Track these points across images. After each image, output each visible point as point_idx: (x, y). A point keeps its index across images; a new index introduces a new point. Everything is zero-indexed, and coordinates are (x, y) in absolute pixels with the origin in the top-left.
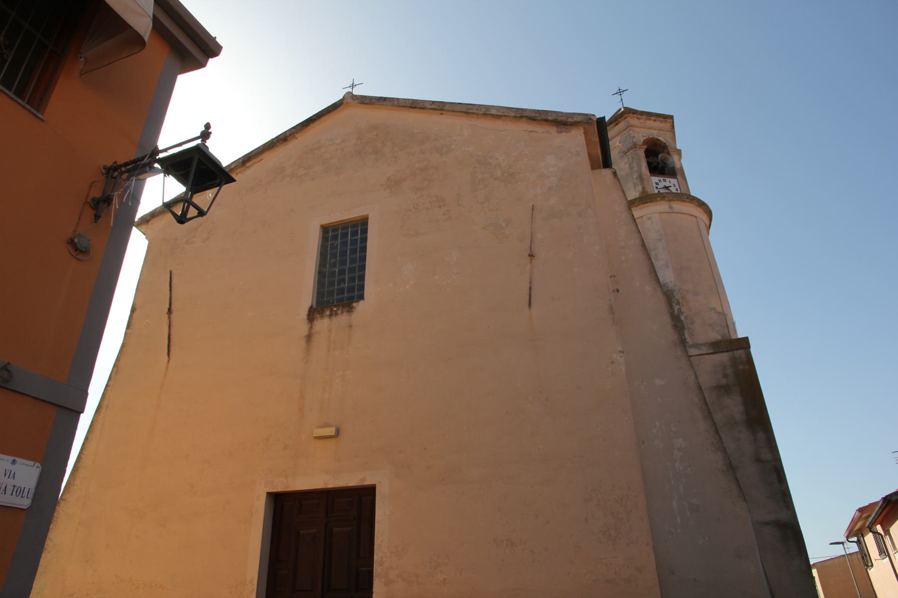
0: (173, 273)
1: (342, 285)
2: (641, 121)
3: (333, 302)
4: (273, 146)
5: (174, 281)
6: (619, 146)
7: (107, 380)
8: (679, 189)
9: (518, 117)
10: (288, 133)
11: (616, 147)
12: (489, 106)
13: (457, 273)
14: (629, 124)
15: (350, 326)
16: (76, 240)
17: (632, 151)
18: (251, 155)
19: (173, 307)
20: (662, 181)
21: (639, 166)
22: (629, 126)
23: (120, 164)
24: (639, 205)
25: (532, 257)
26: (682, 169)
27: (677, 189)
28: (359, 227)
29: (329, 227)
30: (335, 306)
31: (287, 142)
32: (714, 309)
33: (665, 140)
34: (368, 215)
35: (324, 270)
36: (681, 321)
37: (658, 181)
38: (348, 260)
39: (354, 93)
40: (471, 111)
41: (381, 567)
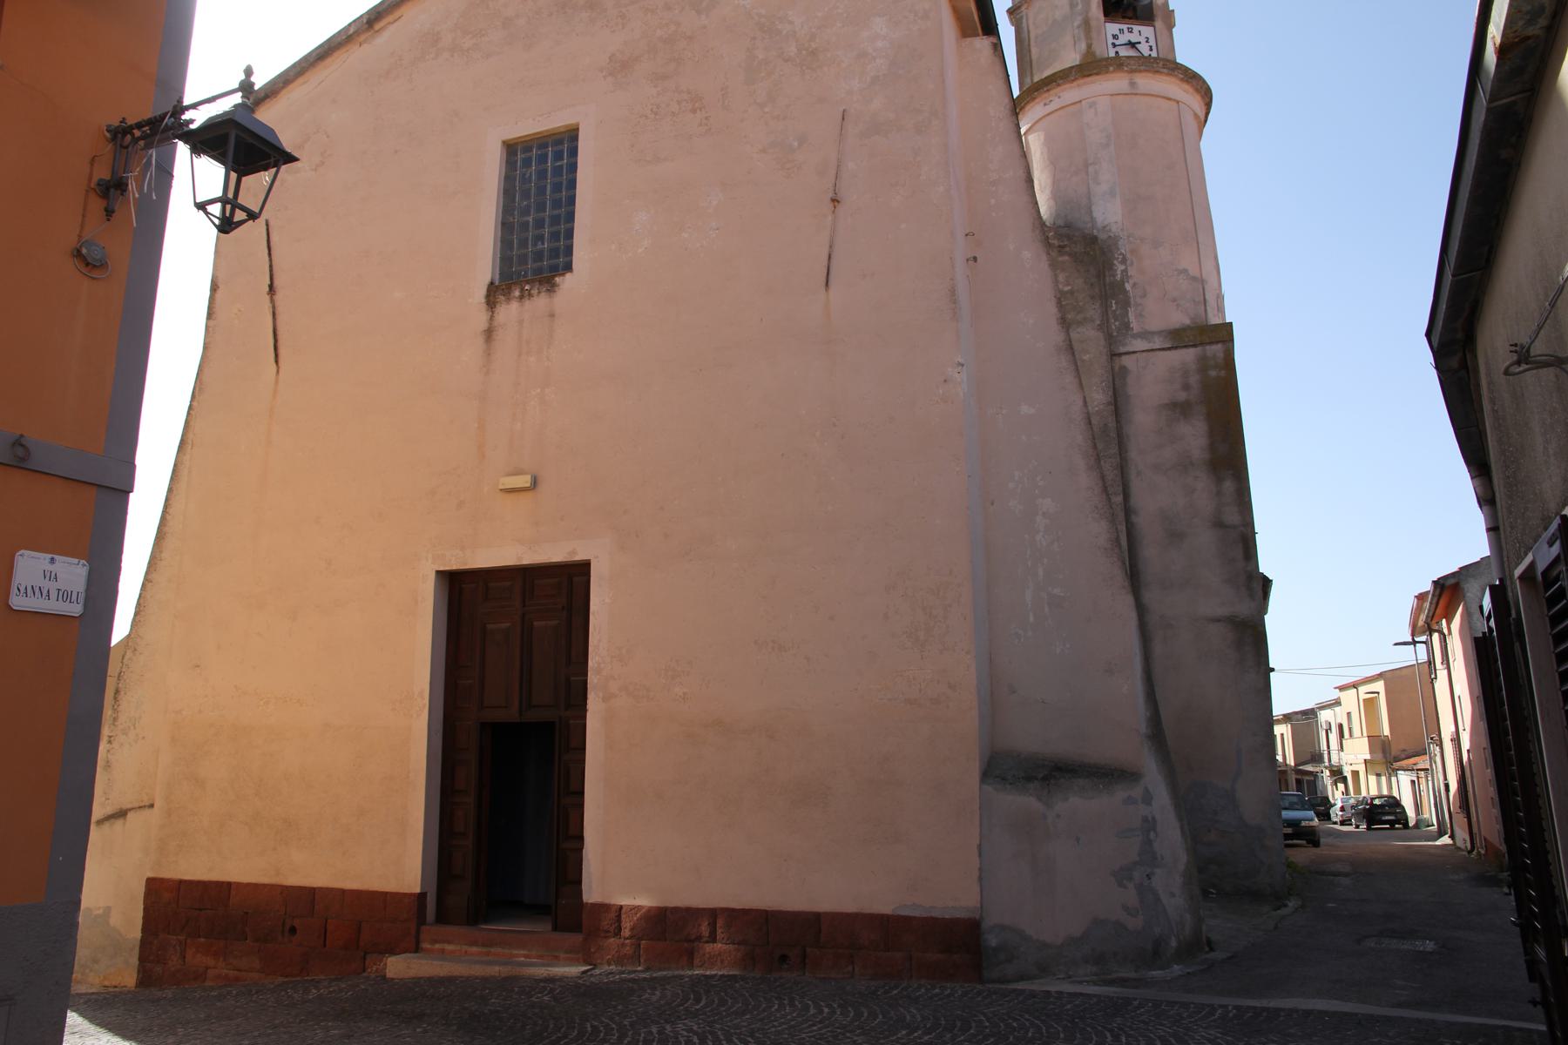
0: (271, 224)
1: (540, 246)
3: (525, 276)
5: (275, 238)
7: (189, 399)
8: (1154, 48)
15: (552, 315)
16: (84, 251)
18: (381, 9)
19: (277, 283)
24: (1076, 79)
25: (836, 204)
27: (1151, 47)
28: (564, 144)
29: (517, 144)
32: (1185, 271)
34: (578, 125)
36: (1125, 292)
37: (1118, 32)
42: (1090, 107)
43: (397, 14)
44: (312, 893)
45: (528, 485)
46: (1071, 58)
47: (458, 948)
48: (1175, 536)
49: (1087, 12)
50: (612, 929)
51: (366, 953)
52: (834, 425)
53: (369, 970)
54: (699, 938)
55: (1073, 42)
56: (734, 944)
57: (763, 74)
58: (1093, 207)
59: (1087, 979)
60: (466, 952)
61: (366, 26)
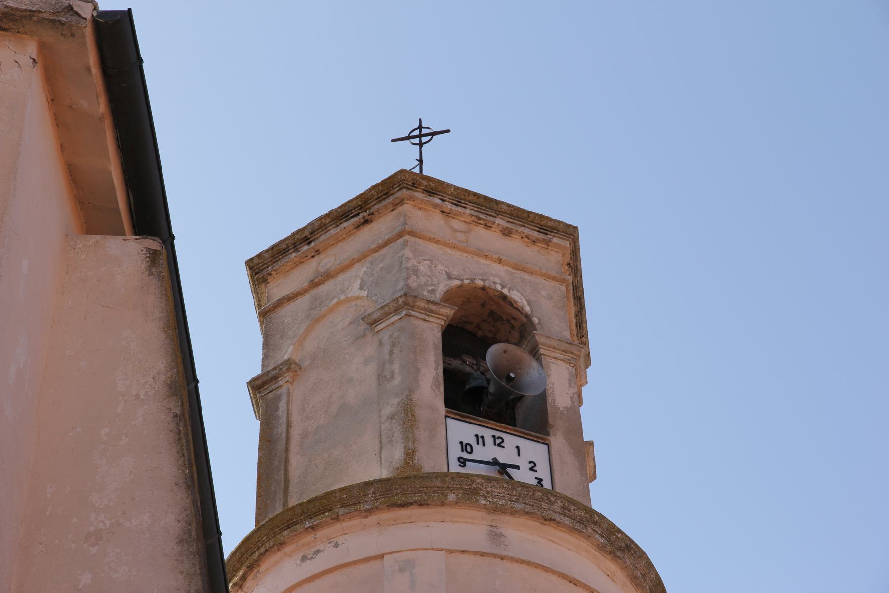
2: (456, 224)
6: (357, 298)
11: (348, 300)
17: (397, 317)
20: (489, 441)
21: (413, 372)
33: (529, 303)
37: (473, 442)
42: (401, 570)
49: (411, 391)
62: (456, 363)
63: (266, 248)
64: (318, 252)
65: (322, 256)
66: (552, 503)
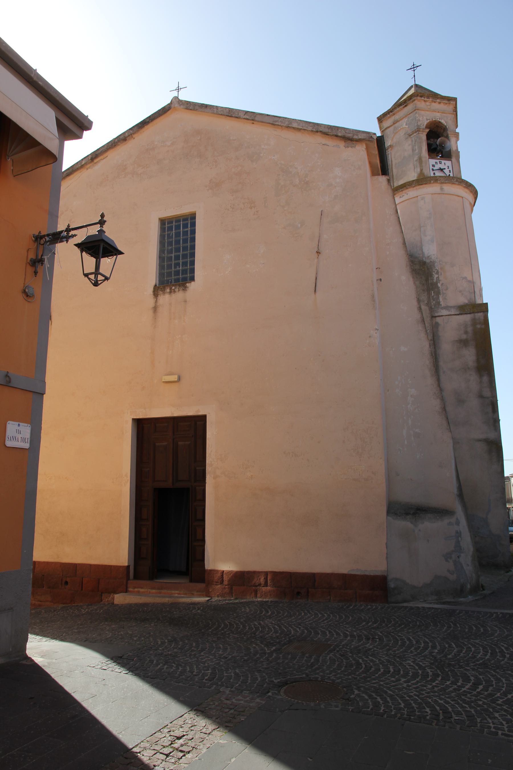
1: (178, 268)
2: (428, 103)
3: (171, 282)
4: (115, 146)
8: (451, 171)
9: (314, 131)
10: (127, 134)
11: (403, 128)
12: (291, 119)
13: (263, 264)
14: (416, 107)
15: (185, 301)
16: (27, 290)
17: (416, 134)
18: (97, 153)
20: (438, 163)
21: (420, 149)
22: (416, 109)
23: (44, 234)
24: (415, 186)
26: (458, 153)
27: (450, 171)
29: (166, 219)
30: (173, 285)
31: (127, 142)
32: (465, 278)
33: (446, 123)
35: (164, 255)
36: (438, 288)
38: (181, 248)
39: (180, 98)
40: (277, 123)
41: (211, 468)
42: (422, 199)
43: (105, 155)
44: (75, 566)
45: (176, 380)
46: (412, 176)
47: (146, 590)
48: (460, 401)
50: (219, 581)
51: (102, 593)
52: (319, 355)
53: (104, 601)
54: (260, 585)
55: (414, 168)
56: (276, 587)
57: (283, 192)
58: (423, 247)
59: (433, 602)
60: (150, 592)
61: (90, 161)
62: (429, 142)
63: (381, 114)
64: (394, 114)
65: (395, 115)
66: (454, 180)
